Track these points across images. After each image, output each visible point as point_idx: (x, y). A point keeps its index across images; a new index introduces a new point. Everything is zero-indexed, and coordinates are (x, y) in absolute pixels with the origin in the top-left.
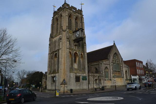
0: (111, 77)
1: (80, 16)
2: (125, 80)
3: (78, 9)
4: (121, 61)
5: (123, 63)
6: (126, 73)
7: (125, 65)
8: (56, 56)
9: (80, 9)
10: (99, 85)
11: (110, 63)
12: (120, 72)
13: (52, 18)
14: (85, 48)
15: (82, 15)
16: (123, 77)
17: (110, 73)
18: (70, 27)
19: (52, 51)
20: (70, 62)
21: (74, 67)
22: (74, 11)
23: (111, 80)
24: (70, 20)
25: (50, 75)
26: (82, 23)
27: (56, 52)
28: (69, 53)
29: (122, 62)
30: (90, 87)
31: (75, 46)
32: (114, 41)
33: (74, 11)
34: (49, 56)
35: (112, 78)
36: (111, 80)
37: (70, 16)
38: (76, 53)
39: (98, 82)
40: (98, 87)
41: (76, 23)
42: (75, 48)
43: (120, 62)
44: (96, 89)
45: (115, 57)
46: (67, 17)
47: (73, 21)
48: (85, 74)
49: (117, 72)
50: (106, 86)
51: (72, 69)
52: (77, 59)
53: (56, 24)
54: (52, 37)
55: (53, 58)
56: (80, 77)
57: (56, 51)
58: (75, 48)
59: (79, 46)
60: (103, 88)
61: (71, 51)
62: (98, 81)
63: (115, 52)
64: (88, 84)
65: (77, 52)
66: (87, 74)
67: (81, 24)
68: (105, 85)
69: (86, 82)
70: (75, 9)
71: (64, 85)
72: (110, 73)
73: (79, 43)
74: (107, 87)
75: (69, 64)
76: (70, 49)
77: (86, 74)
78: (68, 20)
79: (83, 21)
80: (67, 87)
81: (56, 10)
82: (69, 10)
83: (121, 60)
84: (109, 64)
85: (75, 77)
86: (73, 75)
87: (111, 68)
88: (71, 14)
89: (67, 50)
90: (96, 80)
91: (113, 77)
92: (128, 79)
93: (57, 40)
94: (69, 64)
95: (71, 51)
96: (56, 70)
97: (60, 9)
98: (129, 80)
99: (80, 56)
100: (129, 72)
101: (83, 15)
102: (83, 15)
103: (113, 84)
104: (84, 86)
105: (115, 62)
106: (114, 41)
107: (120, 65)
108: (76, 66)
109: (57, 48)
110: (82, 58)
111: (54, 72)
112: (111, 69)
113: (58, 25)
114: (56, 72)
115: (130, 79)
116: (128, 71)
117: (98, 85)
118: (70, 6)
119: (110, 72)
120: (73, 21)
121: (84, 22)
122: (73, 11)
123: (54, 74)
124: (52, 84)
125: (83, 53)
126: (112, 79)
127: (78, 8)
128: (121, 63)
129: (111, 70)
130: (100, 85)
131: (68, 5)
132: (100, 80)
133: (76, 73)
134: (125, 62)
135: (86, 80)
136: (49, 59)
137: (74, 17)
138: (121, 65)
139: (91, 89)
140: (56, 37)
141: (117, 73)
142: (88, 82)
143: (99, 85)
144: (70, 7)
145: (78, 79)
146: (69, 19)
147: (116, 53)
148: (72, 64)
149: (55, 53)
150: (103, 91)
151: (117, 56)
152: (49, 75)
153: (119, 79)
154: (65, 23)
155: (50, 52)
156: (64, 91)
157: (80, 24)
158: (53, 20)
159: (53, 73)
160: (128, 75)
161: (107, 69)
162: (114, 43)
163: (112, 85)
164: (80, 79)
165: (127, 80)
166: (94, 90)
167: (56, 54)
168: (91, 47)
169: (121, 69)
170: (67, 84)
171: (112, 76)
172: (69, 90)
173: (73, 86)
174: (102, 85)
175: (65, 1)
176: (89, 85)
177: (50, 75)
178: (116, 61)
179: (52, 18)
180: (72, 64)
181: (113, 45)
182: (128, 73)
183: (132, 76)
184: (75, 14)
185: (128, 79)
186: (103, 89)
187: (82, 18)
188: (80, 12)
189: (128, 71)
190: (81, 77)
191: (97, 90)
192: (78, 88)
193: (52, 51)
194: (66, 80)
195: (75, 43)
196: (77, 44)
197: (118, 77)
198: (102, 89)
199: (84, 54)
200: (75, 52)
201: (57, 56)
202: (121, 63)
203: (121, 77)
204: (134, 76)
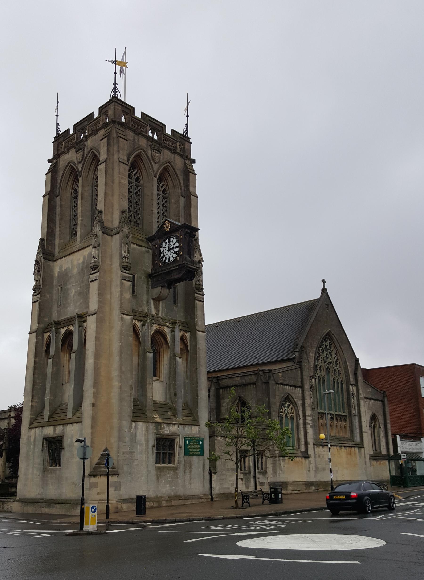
0: (306, 444)
1: (178, 162)
2: (368, 457)
3: (173, 131)
4: (351, 370)
5: (360, 378)
6: (373, 427)
7: (370, 390)
8: (71, 346)
9: (181, 131)
10: (255, 477)
11: (305, 377)
12: (347, 417)
13: (49, 161)
14: (199, 314)
15: (189, 159)
16: (360, 446)
17: (305, 424)
18: (133, 215)
19: (47, 319)
20: (134, 373)
21: (149, 394)
22: (156, 137)
23: (306, 455)
24: (137, 179)
25: (38, 434)
26: (189, 196)
27: (71, 328)
28: (131, 332)
29: (355, 375)
30: (217, 489)
31: (157, 300)
32: (324, 282)
33: (156, 137)
34: (34, 341)
35: (311, 446)
36: (306, 455)
37: (135, 164)
38: (159, 333)
39: (252, 465)
40: (252, 488)
41: (164, 195)
42: (154, 312)
43: (347, 376)
44: (245, 497)
45: (325, 353)
46: (125, 169)
47: (151, 188)
48: (195, 430)
49: (332, 419)
50: (285, 484)
51: (139, 411)
52: (165, 359)
53: (68, 194)
54: (47, 253)
55: (52, 352)
56: (177, 440)
57: (69, 321)
58: (157, 308)
59: (175, 303)
60: (275, 495)
61: (139, 324)
62: (250, 461)
63: (326, 331)
64: (210, 474)
65: (166, 330)
66: (205, 431)
67: (182, 200)
68: (281, 478)
69: (199, 464)
70: (159, 127)
71: (103, 480)
72: (305, 424)
73: (172, 290)
74: (290, 488)
75: (130, 382)
76: (136, 314)
77: (201, 430)
78: (127, 182)
79: (191, 189)
80: (117, 487)
81: (68, 124)
82: (130, 135)
83: (353, 364)
84: (299, 384)
85: (152, 442)
86: (143, 434)
87: (308, 402)
88: (139, 156)
89: (122, 319)
90: (243, 454)
91: (319, 443)
92: (384, 452)
93: (75, 271)
94: (130, 382)
95: (139, 324)
96: (70, 408)
97: (87, 124)
98: (389, 458)
99: (178, 346)
100: (388, 421)
101: (194, 161)
102: (194, 161)
103: (315, 476)
104: (190, 479)
105: (324, 372)
106: (324, 282)
107: (348, 390)
108: (157, 391)
109: (72, 310)
110: (185, 357)
111: (57, 416)
112: (306, 405)
113: (76, 198)
114: (70, 415)
115: (392, 453)
116: (380, 418)
117: (252, 480)
118: (138, 114)
119: (301, 421)
120: (151, 188)
121: (199, 192)
122: (148, 138)
123: (59, 429)
124: (44, 470)
125: (188, 335)
126: (311, 452)
127: (173, 124)
128: (352, 380)
129: (309, 412)
130: (261, 478)
131: (129, 110)
132: (261, 454)
133: (160, 423)
134: (368, 374)
135: (202, 454)
136: (36, 356)
137: (156, 167)
138: (353, 389)
139: (226, 496)
140: (69, 258)
141: (331, 426)
142: (207, 462)
143: (255, 477)
144: (136, 118)
145: (164, 449)
146: (130, 176)
147: (328, 337)
148: (142, 385)
149: (63, 331)
150: (274, 505)
151: (336, 347)
152: (33, 431)
153: (343, 452)
154: (111, 195)
155: (39, 323)
156: (108, 507)
157: (178, 202)
158: (53, 172)
159: (53, 421)
160: (382, 434)
161: (288, 406)
162: (324, 290)
163: (312, 479)
164: (177, 449)
165: (376, 457)
166: (240, 502)
167: (69, 334)
168: (230, 291)
169: (349, 405)
170: (120, 471)
171: (310, 440)
172: (128, 501)
173: (141, 478)
174: (270, 478)
175: (115, 90)
176: (214, 477)
177: (38, 431)
178: (328, 372)
179: (49, 161)
180: (142, 385)
181: (318, 297)
182: (382, 427)
183: (402, 438)
184: (157, 156)
185: (384, 452)
186: (277, 496)
187: (188, 173)
188: (180, 143)
189: (380, 418)
190: (180, 443)
191: (251, 501)
192: (165, 489)
193: (47, 319)
194: (113, 454)
195: (157, 291)
196: (165, 292)
197: (338, 442)
198: (273, 496)
199: (194, 337)
200: (155, 327)
201: (75, 346)
202: (352, 380)
203: (349, 442)
204: (408, 443)
